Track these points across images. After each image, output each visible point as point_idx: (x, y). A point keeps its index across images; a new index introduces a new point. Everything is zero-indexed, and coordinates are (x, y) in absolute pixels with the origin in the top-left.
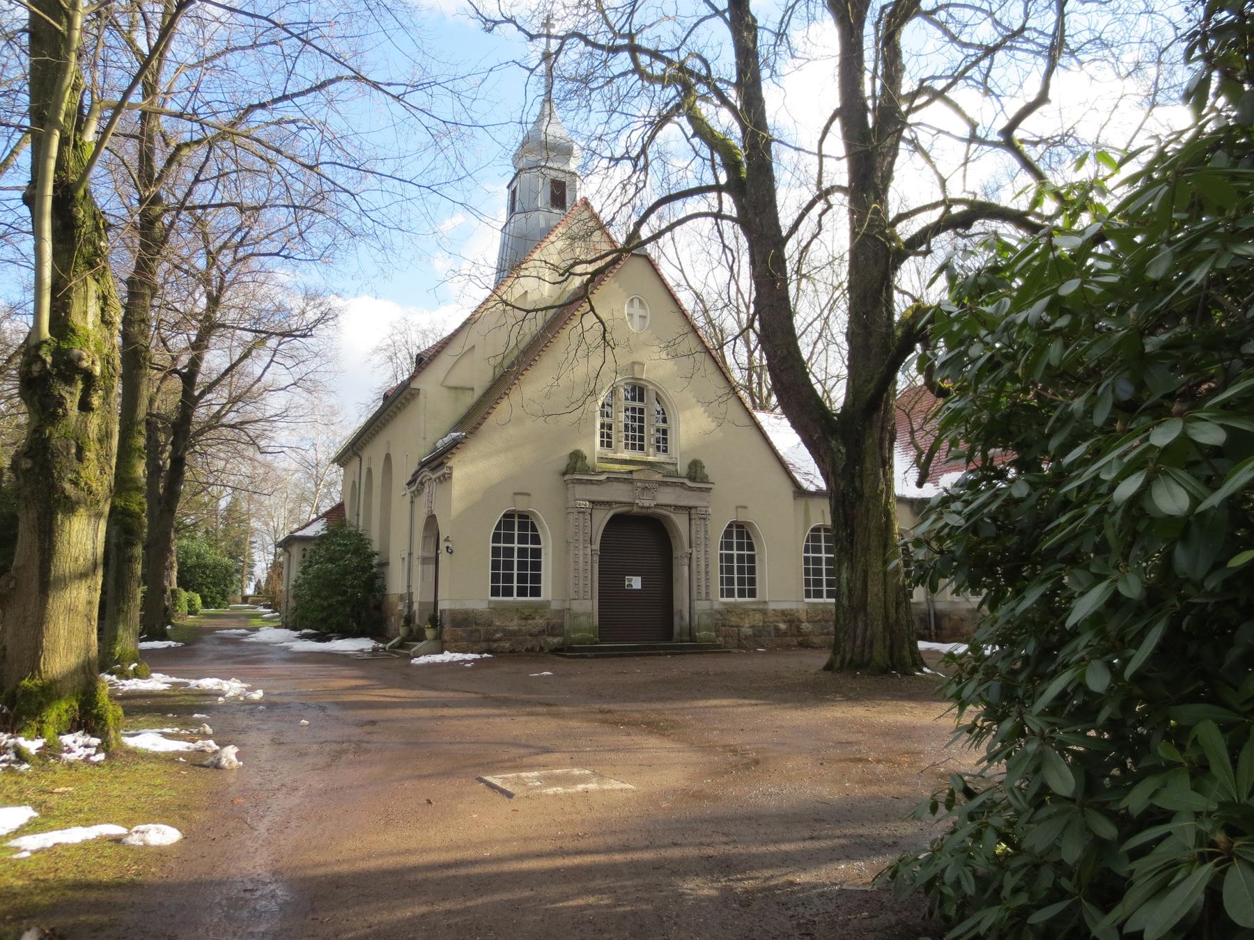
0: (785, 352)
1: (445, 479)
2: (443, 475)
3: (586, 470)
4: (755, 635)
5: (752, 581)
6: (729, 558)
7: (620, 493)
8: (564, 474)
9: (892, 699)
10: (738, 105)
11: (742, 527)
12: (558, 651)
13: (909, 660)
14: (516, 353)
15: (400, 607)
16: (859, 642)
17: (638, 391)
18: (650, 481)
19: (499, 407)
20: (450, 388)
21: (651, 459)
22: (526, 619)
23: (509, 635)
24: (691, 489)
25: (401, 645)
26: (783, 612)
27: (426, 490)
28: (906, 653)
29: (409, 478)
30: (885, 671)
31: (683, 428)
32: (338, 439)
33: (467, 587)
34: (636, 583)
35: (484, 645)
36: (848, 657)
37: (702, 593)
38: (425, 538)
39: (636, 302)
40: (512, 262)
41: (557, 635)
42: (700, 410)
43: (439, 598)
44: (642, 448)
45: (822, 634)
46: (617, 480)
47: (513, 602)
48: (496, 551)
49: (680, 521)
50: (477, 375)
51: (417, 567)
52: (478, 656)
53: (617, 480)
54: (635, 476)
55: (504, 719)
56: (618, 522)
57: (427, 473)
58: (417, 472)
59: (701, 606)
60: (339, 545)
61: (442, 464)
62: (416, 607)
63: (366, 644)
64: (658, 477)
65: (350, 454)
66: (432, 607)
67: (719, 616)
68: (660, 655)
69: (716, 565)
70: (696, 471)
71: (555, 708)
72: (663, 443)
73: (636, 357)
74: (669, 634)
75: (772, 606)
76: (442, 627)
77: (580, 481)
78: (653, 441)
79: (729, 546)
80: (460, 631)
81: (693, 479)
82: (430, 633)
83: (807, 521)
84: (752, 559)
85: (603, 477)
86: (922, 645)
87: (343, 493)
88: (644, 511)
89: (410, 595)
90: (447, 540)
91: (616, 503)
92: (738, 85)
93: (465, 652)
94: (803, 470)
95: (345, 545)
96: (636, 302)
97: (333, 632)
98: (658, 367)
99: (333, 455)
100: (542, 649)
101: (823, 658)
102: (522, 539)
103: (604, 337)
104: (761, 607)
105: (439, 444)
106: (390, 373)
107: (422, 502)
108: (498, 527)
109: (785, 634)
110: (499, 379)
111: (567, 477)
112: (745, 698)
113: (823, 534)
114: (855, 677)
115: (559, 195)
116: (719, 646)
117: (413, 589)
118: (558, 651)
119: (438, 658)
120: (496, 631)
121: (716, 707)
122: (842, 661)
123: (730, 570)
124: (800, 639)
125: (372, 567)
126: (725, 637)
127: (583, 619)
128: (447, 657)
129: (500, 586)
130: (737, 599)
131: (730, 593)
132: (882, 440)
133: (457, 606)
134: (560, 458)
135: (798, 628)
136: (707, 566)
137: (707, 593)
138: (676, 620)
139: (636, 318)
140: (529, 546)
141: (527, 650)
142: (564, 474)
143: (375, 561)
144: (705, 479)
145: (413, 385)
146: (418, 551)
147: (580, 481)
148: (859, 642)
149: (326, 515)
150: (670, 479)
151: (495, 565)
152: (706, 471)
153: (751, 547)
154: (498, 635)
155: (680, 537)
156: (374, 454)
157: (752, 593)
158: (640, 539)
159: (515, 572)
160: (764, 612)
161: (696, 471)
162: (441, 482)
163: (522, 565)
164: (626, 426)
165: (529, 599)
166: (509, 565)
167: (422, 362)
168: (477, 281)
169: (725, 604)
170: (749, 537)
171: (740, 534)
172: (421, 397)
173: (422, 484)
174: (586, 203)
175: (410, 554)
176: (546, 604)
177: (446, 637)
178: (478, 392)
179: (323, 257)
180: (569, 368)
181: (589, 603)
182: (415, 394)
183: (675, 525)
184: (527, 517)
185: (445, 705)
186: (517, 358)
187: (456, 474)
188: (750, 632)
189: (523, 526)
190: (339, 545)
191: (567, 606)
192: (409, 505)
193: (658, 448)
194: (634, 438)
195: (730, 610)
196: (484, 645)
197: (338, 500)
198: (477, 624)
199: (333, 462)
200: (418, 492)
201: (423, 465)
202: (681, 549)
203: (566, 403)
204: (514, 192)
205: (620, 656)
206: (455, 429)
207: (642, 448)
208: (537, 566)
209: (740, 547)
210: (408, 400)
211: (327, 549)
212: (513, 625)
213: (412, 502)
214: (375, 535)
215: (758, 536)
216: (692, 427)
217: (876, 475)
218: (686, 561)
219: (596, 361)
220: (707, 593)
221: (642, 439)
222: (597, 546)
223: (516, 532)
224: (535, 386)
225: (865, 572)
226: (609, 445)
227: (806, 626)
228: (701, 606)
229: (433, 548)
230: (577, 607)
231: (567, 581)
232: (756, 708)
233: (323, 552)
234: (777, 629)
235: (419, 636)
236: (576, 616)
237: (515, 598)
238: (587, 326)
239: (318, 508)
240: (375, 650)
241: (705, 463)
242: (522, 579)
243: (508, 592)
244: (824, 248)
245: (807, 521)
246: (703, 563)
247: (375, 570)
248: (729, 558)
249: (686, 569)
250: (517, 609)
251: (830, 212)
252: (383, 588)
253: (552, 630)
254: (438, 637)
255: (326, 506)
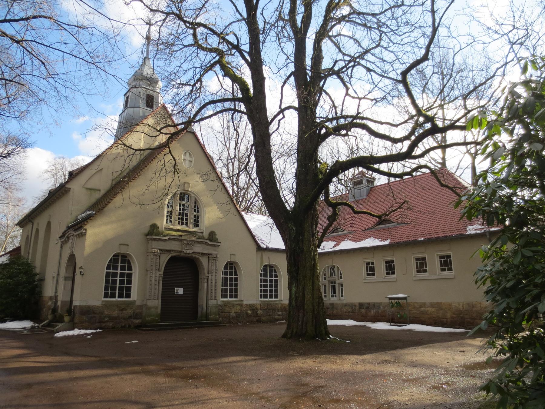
0: (269, 179)
1: (82, 235)
2: (81, 233)
3: (160, 234)
4: (237, 316)
5: (236, 290)
6: (226, 279)
7: (175, 246)
8: (147, 235)
9: (322, 354)
10: (250, 60)
11: (232, 264)
12: (139, 327)
13: (324, 332)
14: (128, 170)
15: (49, 304)
16: (300, 323)
17: (184, 195)
18: (190, 241)
19: (115, 200)
20: (87, 189)
21: (191, 230)
22: (122, 310)
23: (112, 319)
24: (210, 245)
25: (49, 325)
26: (250, 306)
27: (70, 241)
28: (322, 328)
29: (61, 234)
30: (313, 338)
31: (207, 215)
32: (20, 214)
33: (90, 293)
34: (180, 291)
35: (98, 325)
36: (295, 330)
37: (213, 295)
38: (67, 266)
39: (188, 154)
40: (127, 126)
41: (137, 319)
42: (215, 207)
43: (74, 299)
44: (186, 224)
45: (267, 316)
46: (174, 239)
47: (116, 301)
48: (108, 274)
49: (204, 261)
50: (103, 184)
51: (62, 282)
52: (94, 331)
53: (174, 239)
54: (183, 238)
55: (117, 378)
56: (173, 260)
57: (71, 232)
58: (65, 231)
59: (212, 302)
60: (16, 269)
61: (81, 227)
62: (59, 303)
63: (27, 324)
64: (194, 239)
65: (26, 221)
66: (69, 304)
67: (220, 308)
68: (191, 328)
69: (220, 282)
70: (212, 236)
71: (145, 367)
72: (197, 223)
73: (186, 180)
74: (196, 318)
75: (245, 302)
76: (74, 315)
77: (155, 239)
78: (192, 221)
79: (225, 273)
80: (85, 318)
81: (211, 241)
82: (67, 319)
83: (262, 262)
84: (236, 279)
85: (167, 238)
86: (330, 322)
87: (21, 242)
88: (187, 255)
89: (56, 297)
90: (81, 268)
91: (173, 251)
92: (249, 53)
93: (87, 329)
94: (260, 238)
95: (20, 269)
96: (188, 154)
97: (7, 317)
98: (197, 185)
99: (17, 222)
100: (130, 326)
101: (281, 329)
102: (123, 268)
103: (175, 167)
104: (240, 303)
105: (80, 217)
106: (53, 183)
107: (69, 245)
108: (110, 262)
109: (250, 316)
110: (114, 187)
111: (148, 237)
112: (248, 355)
113: (268, 268)
114: (299, 341)
115: (150, 101)
116: (220, 323)
117: (58, 294)
118: (139, 327)
119: (71, 333)
120: (105, 317)
121: (235, 362)
122: (292, 333)
123: (226, 285)
124: (257, 318)
125: (35, 281)
126: (223, 318)
127: (153, 310)
128: (76, 332)
129: (109, 292)
130: (229, 299)
131: (225, 296)
132: (312, 224)
133: (84, 304)
134: (146, 228)
135: (256, 313)
136: (216, 283)
137: (215, 296)
138: (199, 310)
139: (187, 162)
140: (126, 272)
141: (122, 327)
142: (147, 235)
143: (37, 278)
144: (216, 241)
145: (67, 186)
146: (63, 273)
147: (155, 239)
148: (300, 323)
149: (10, 252)
150: (200, 240)
151: (107, 282)
152: (217, 237)
153: (276, 276)
154: (106, 319)
155: (203, 268)
156: (41, 222)
157: (236, 296)
158: (183, 269)
159: (118, 285)
160: (241, 305)
161: (212, 236)
162: (79, 237)
163: (122, 282)
164: (180, 213)
165: (124, 299)
166: (114, 282)
167: (73, 175)
168: (109, 132)
169: (223, 301)
170: (235, 269)
171: (232, 267)
172: (71, 192)
173: (68, 238)
174: (164, 107)
175: (58, 275)
176: (134, 302)
177: (76, 321)
178: (103, 192)
179: (21, 116)
180: (156, 180)
181: (157, 301)
182: (67, 191)
183: (201, 263)
184: (126, 257)
185: (79, 367)
186: (128, 174)
187: (89, 233)
188: (234, 315)
189: (123, 262)
190: (16, 269)
191: (144, 303)
192: (59, 249)
193: (195, 224)
194: (183, 219)
195: (225, 304)
196: (98, 325)
197: (18, 245)
198: (94, 313)
199: (17, 225)
200: (63, 243)
201: (69, 228)
202: (203, 275)
203: (149, 201)
204: (127, 98)
205: (172, 329)
206: (88, 210)
207: (186, 224)
208: (129, 282)
209: (271, 276)
210: (63, 194)
211: (8, 271)
212: (115, 314)
213: (61, 247)
214: (38, 263)
215: (240, 269)
216: (211, 215)
217: (310, 241)
218: (206, 280)
219: (169, 180)
220: (215, 296)
221: (187, 220)
222: (162, 272)
223: (119, 264)
224: (135, 190)
225: (304, 289)
226: (171, 221)
227: (260, 312)
228: (212, 302)
229: (71, 272)
230: (150, 303)
231: (144, 289)
232: (257, 362)
233: (5, 273)
234: (247, 313)
235: (60, 320)
236: (150, 308)
237: (117, 299)
238: (166, 161)
239: (5, 249)
240: (32, 327)
241: (217, 233)
242: (121, 289)
243: (113, 296)
244: (286, 133)
245: (262, 262)
246: (214, 281)
247: (36, 283)
248: (226, 279)
249: (206, 284)
250: (118, 305)
251: (284, 119)
252: (40, 293)
253: (136, 316)
254: (72, 321)
255: (10, 248)
